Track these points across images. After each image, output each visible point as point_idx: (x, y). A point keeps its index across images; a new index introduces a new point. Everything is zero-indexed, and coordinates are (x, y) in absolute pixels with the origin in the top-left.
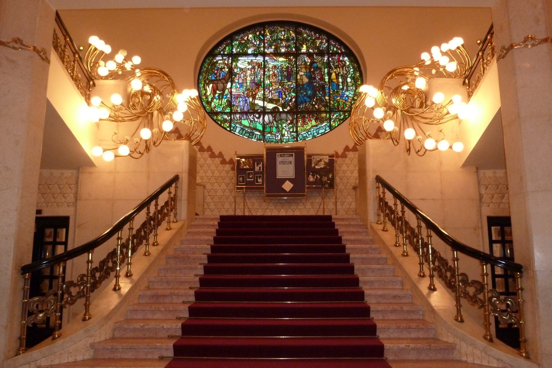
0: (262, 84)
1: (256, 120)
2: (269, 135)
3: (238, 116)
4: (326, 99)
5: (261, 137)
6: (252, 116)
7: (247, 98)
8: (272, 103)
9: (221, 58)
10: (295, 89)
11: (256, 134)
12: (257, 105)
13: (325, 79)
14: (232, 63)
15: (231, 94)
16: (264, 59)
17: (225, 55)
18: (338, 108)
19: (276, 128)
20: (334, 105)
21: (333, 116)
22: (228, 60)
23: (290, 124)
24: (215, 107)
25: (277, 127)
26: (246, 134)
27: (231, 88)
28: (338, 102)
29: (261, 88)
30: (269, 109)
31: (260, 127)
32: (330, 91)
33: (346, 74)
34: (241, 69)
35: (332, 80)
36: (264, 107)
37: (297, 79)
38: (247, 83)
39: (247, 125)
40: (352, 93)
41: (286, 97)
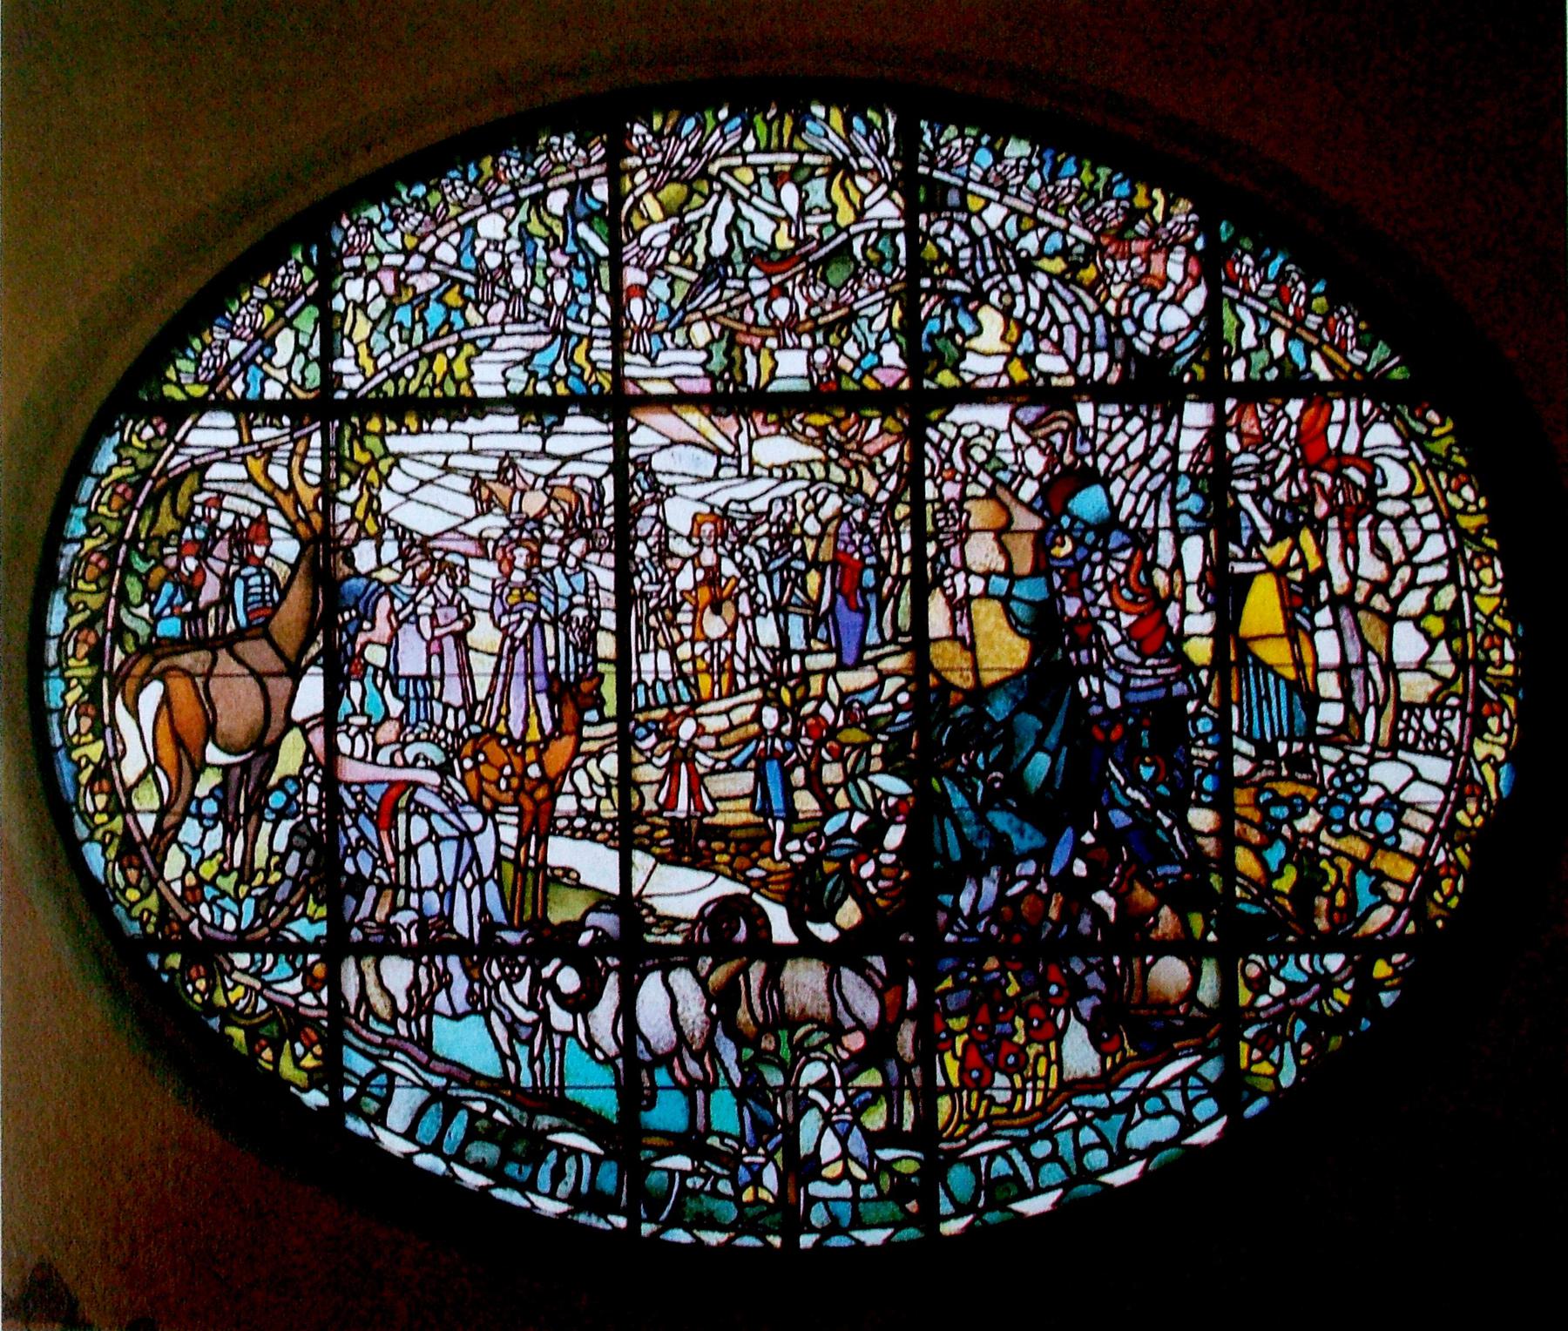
0: (609, 690)
1: (561, 1019)
2: (682, 1162)
3: (398, 973)
4: (1190, 834)
5: (608, 1178)
6: (522, 989)
7: (474, 820)
8: (701, 862)
9: (231, 439)
10: (900, 739)
11: (566, 1152)
12: (568, 878)
13: (1181, 638)
14: (328, 492)
15: (331, 784)
16: (621, 442)
17: (273, 410)
18: (1306, 912)
19: (741, 1095)
20: (1263, 888)
21: (1259, 986)
22: (298, 454)
23: (861, 1061)
24: (192, 896)
25: (750, 1092)
26: (477, 1151)
27: (329, 719)
28: (1303, 855)
29: (599, 732)
30: (671, 923)
31: (593, 1087)
32: (1226, 753)
33: (1379, 587)
34: (416, 546)
35: (1244, 645)
36: (627, 904)
37: (918, 640)
38: (465, 671)
39: (486, 1062)
40: (1438, 769)
41: (829, 809)
